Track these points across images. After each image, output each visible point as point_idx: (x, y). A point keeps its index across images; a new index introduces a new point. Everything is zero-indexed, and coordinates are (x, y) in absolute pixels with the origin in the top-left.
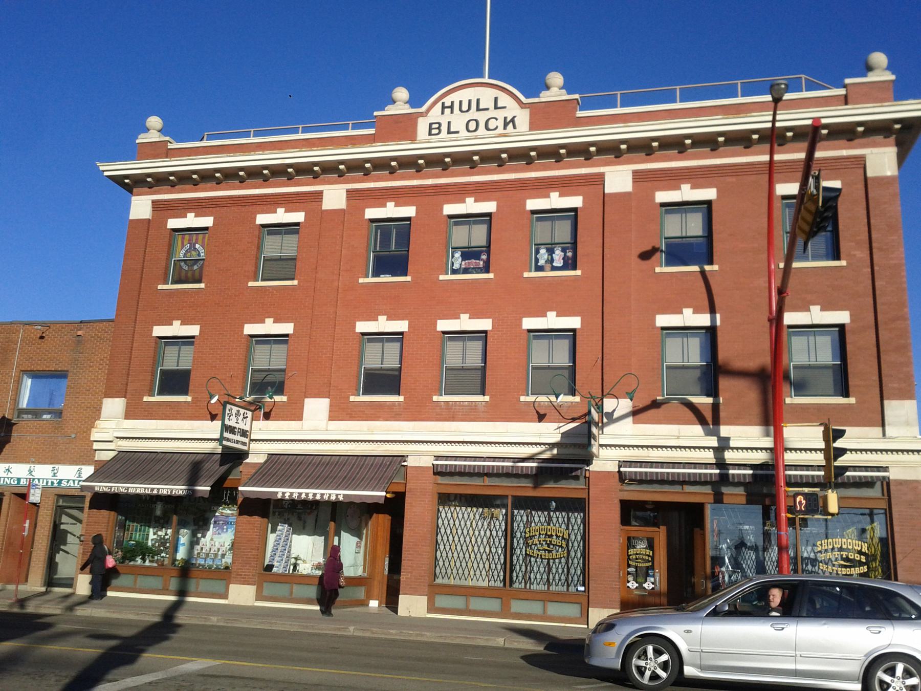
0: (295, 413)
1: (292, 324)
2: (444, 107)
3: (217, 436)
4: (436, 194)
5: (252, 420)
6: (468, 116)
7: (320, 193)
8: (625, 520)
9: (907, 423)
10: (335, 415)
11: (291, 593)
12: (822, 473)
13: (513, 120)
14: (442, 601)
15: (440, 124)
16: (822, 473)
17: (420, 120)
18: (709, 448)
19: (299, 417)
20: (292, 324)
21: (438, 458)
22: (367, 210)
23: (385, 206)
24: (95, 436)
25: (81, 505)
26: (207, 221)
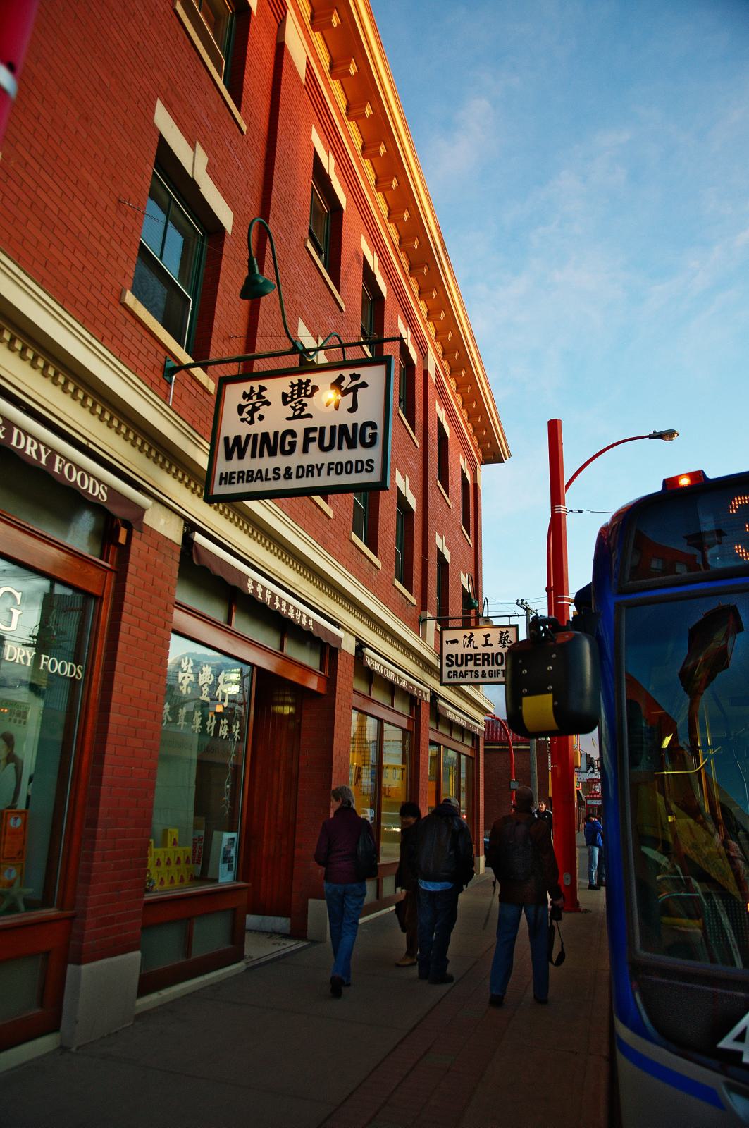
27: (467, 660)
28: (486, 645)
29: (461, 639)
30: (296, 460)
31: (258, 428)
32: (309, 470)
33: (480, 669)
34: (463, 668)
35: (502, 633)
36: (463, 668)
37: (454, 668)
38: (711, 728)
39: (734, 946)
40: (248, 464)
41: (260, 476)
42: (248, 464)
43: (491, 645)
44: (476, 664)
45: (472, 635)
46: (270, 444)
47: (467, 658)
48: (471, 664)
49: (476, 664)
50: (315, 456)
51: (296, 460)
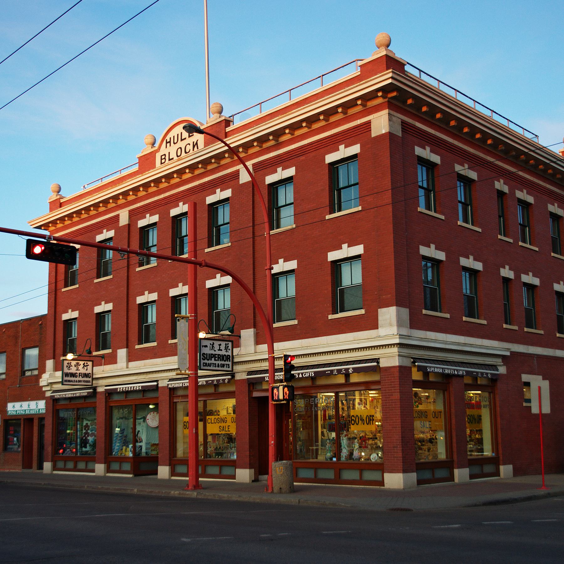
0: (112, 359)
1: (112, 304)
2: (167, 143)
3: (61, 380)
4: (166, 204)
5: (93, 366)
6: (177, 146)
7: (369, 123)
8: (530, 400)
9: (391, 325)
10: (131, 358)
11: (543, 481)
12: (91, 390)
13: (197, 144)
14: (115, 466)
15: (165, 155)
16: (91, 390)
17: (157, 154)
18: (394, 345)
19: (375, 326)
20: (112, 304)
21: (250, 373)
22: (327, 157)
23: (215, 193)
24: (41, 384)
25: (36, 423)
26: (291, 172)
27: (212, 357)
28: (220, 350)
29: (209, 346)
30: (78, 379)
31: (70, 371)
32: (80, 381)
33: (217, 362)
34: (210, 362)
35: (226, 344)
36: (210, 362)
37: (206, 361)
38: (276, 404)
39: (240, 496)
40: (69, 378)
41: (71, 381)
42: (69, 378)
43: (221, 350)
44: (215, 360)
45: (213, 344)
46: (73, 375)
47: (212, 356)
48: (213, 359)
49: (215, 360)
50: (81, 379)
51: (78, 379)
